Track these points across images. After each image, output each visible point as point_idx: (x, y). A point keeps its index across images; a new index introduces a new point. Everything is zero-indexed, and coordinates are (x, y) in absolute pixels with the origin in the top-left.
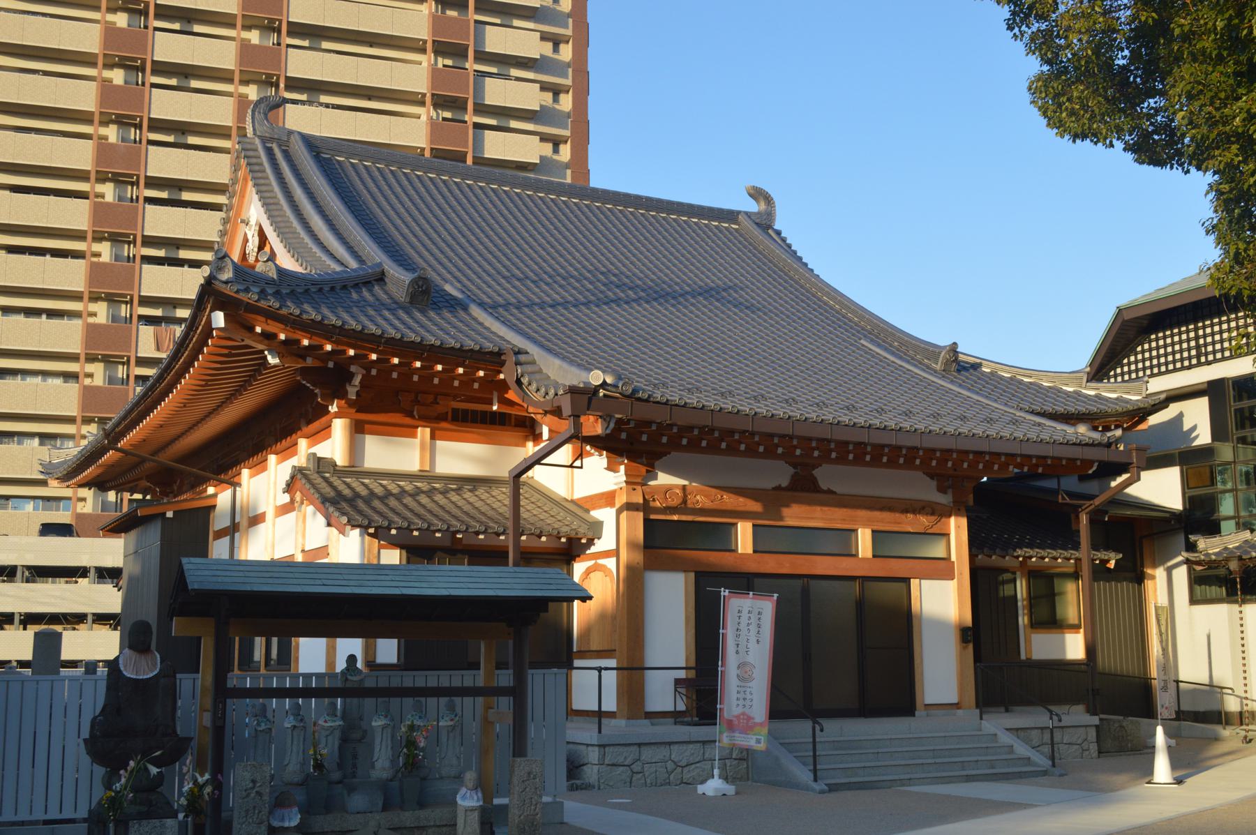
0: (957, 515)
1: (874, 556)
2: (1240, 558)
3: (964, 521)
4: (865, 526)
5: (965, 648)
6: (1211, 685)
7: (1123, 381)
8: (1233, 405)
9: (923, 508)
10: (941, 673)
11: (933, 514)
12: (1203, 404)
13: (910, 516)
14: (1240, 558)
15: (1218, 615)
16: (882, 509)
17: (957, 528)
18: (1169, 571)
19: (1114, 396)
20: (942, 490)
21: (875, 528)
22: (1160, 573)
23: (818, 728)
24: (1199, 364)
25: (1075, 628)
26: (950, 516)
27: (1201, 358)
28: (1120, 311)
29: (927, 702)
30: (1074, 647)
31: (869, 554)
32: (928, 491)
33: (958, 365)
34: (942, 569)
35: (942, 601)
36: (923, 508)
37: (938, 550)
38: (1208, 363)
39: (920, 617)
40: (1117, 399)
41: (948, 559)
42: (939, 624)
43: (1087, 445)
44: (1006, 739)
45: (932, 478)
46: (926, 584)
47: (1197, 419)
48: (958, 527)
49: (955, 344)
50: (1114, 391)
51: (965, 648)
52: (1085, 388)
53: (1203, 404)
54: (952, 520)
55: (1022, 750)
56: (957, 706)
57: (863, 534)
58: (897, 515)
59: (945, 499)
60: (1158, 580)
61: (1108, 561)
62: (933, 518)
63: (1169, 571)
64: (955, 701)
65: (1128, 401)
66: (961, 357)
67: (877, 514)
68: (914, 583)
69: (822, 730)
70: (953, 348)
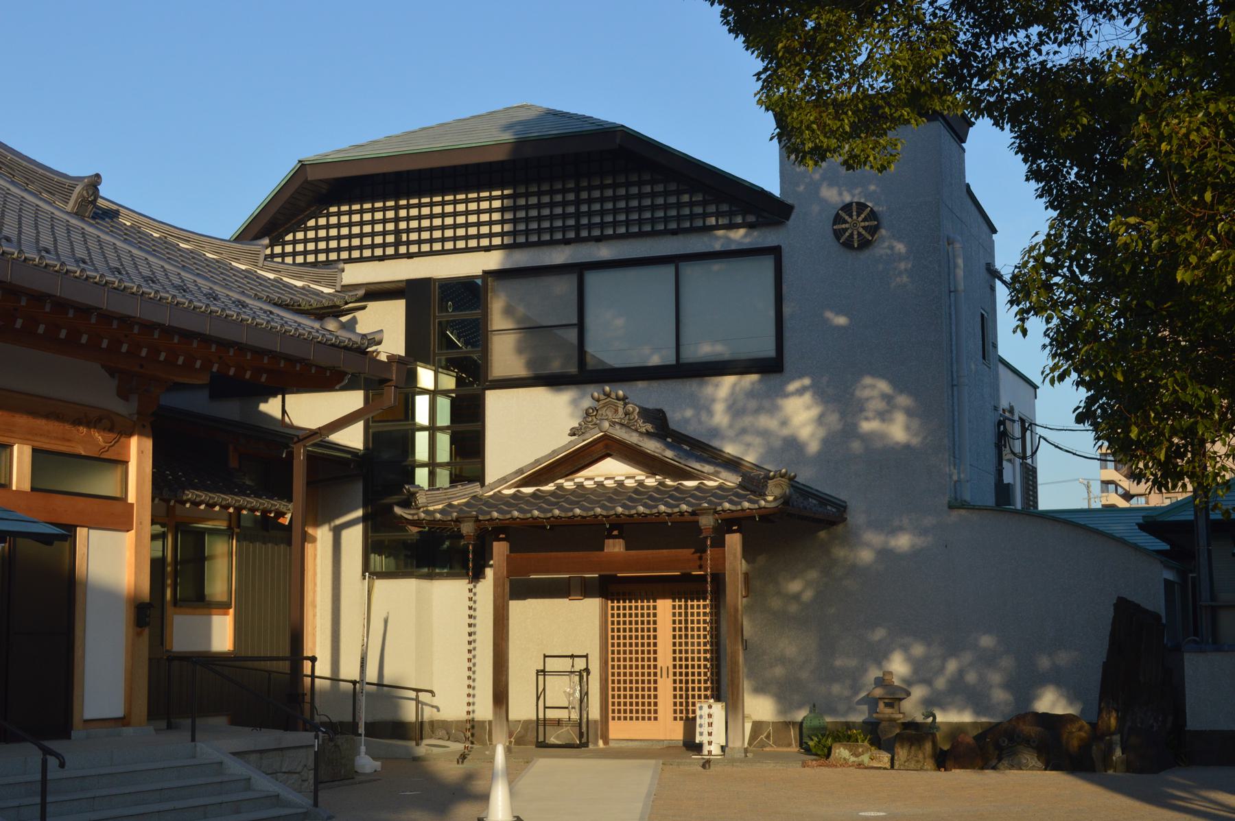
0: (141, 434)
1: (33, 489)
2: (477, 520)
3: (148, 444)
4: (24, 440)
5: (139, 634)
6: (380, 685)
7: (294, 263)
8: (437, 316)
9: (100, 420)
10: (105, 676)
11: (111, 430)
12: (397, 309)
13: (83, 430)
14: (477, 520)
15: (398, 595)
16: (48, 416)
17: (138, 452)
18: (337, 532)
19: (299, 284)
20: (123, 394)
21: (37, 444)
22: (323, 535)
23: (52, 762)
24: (397, 256)
25: (223, 607)
26: (131, 435)
27: (399, 249)
28: (303, 166)
29: (87, 716)
30: (222, 634)
31: (27, 487)
32: (105, 396)
33: (92, 206)
34: (114, 515)
35: (114, 561)
36: (100, 420)
37: (105, 485)
38: (409, 256)
39: (85, 584)
40: (303, 288)
41: (123, 499)
42: (109, 595)
43: (345, 348)
44: (237, 768)
45: (112, 375)
46: (95, 534)
47: (387, 327)
48: (141, 452)
49: (98, 176)
50: (299, 278)
51: (139, 634)
52: (262, 268)
53: (397, 309)
54: (134, 441)
55: (264, 784)
56: (123, 721)
57: (20, 452)
58: (68, 427)
59: (123, 408)
60: (319, 543)
61: (283, 514)
62: (112, 435)
63: (337, 532)
64: (120, 713)
65: (319, 294)
66: (100, 202)
67: (41, 423)
68: (81, 532)
69: (62, 765)
70: (94, 182)
